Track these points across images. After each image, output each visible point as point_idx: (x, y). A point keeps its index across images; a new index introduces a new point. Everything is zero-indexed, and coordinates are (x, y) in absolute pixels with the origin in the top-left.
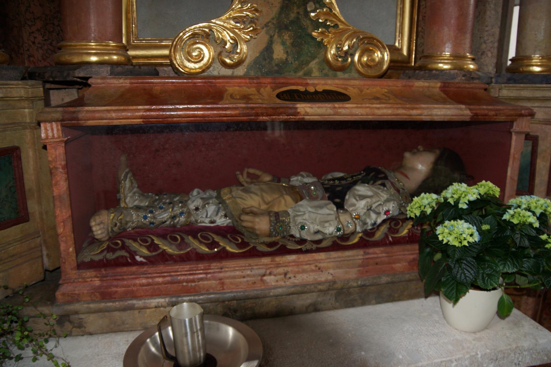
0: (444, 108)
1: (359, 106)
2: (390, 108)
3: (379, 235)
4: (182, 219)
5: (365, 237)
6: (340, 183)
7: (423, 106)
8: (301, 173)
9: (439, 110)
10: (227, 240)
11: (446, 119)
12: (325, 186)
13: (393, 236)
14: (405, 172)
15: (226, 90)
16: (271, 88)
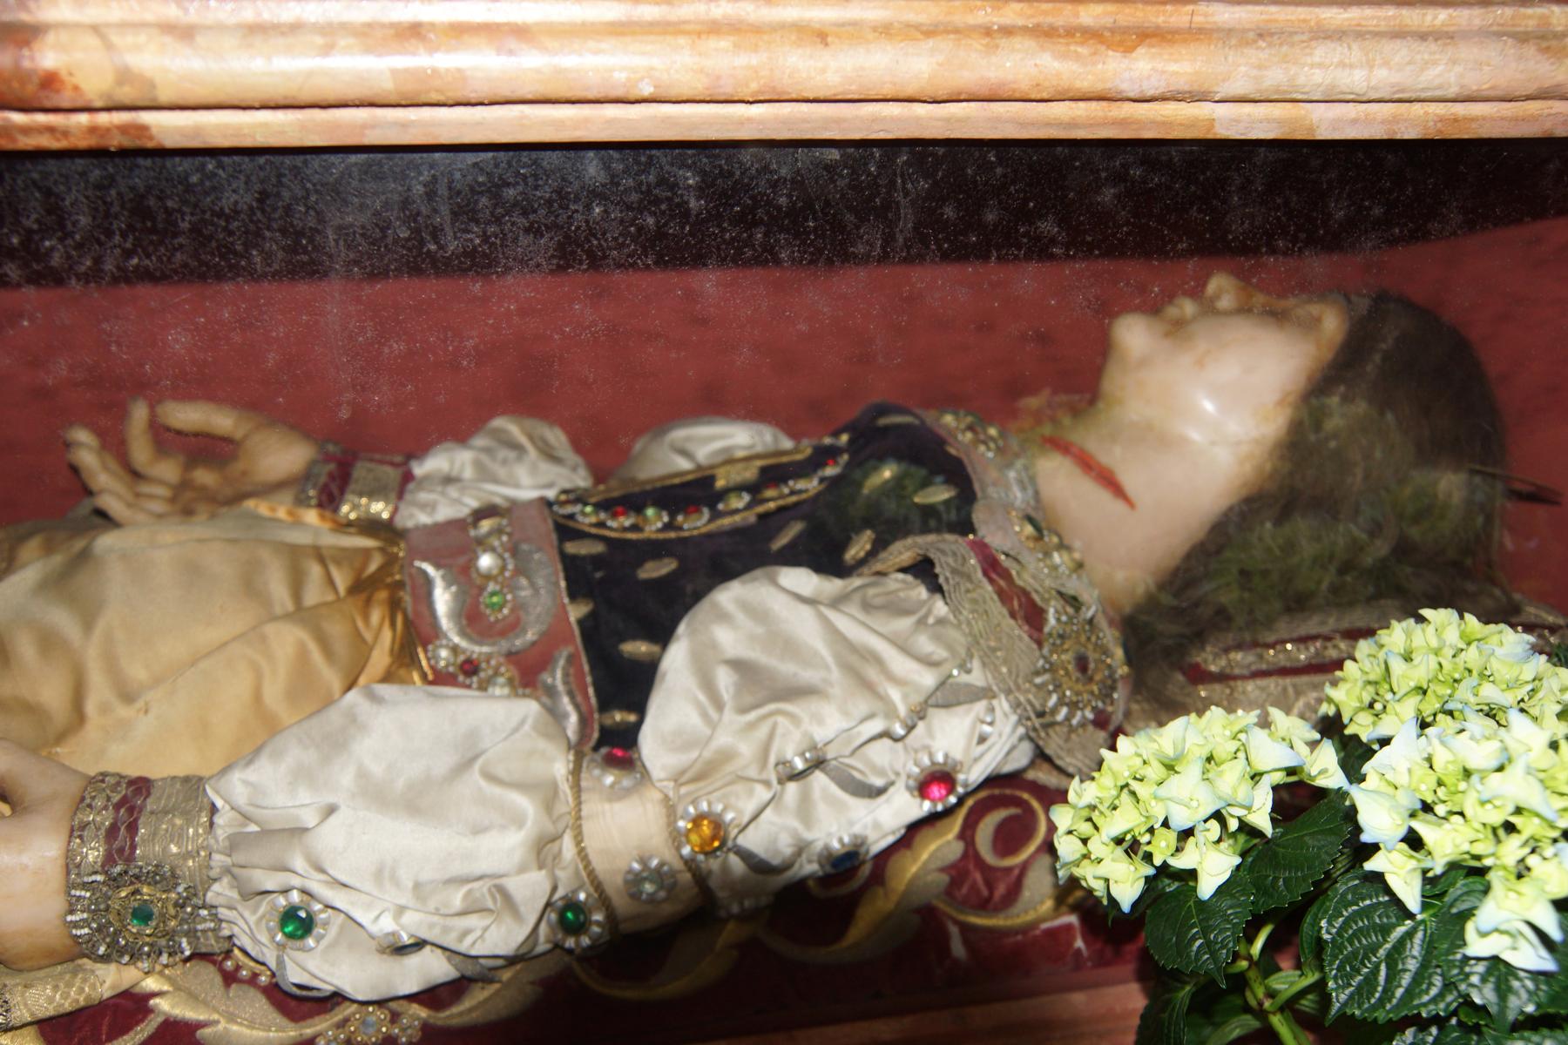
0: (1399, 34)
2: (930, 32)
6: (668, 527)
8: (499, 422)
9: (1355, 52)
11: (1412, 123)
12: (572, 548)
14: (1112, 456)
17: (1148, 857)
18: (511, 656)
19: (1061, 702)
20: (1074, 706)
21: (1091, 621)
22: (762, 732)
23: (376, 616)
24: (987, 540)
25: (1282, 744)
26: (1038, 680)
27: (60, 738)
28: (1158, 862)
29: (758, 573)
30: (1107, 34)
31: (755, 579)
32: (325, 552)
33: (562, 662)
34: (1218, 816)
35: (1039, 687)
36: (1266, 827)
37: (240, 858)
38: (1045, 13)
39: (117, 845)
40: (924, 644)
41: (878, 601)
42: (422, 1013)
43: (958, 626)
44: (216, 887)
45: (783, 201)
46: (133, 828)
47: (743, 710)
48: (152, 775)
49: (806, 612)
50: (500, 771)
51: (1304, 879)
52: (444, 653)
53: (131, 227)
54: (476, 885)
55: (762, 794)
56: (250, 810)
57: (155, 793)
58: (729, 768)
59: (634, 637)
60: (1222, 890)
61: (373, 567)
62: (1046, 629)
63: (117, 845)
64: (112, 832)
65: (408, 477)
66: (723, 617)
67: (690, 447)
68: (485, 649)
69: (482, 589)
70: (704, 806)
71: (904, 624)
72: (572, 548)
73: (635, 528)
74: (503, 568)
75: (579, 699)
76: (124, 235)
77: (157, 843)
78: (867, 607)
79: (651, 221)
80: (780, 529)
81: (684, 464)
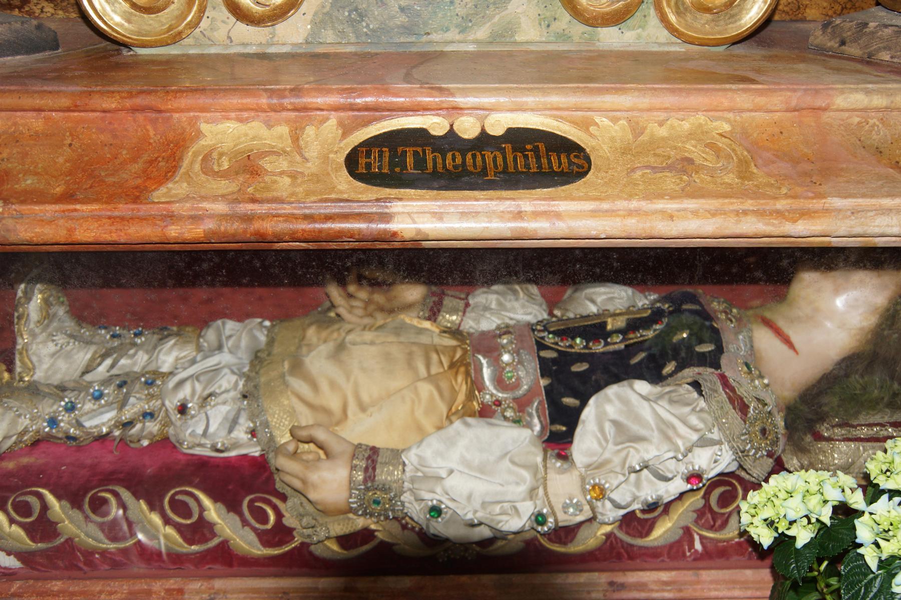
1: (605, 206)
3: (663, 531)
4: (153, 427)
5: (622, 535)
6: (586, 347)
7: (837, 202)
10: (237, 518)
12: (543, 354)
13: (705, 533)
15: (199, 134)
16: (341, 124)
17: (776, 529)
18: (515, 399)
19: (752, 447)
20: (758, 449)
21: (770, 412)
22: (623, 454)
23: (460, 378)
24: (726, 374)
25: (839, 488)
26: (743, 438)
27: (338, 423)
28: (780, 531)
29: (625, 383)
30: (787, 214)
31: (623, 386)
32: (438, 348)
33: (536, 404)
34: (807, 516)
35: (743, 441)
36: (828, 522)
37: (416, 486)
38: (762, 204)
39: (368, 474)
40: (694, 420)
41: (675, 399)
42: (478, 549)
43: (709, 413)
44: (405, 495)
45: (650, 264)
46: (374, 469)
47: (616, 444)
48: (377, 446)
49: (645, 404)
50: (516, 460)
51: (840, 546)
52: (488, 397)
53: (407, 269)
54: (505, 504)
55: (622, 478)
56: (419, 467)
57: (381, 454)
58: (609, 466)
59: (568, 396)
60: (805, 546)
61: (458, 355)
62: (749, 415)
63: (368, 474)
64: (366, 469)
65: (467, 305)
66: (609, 400)
67: (594, 297)
68: (505, 396)
69: (504, 369)
70: (597, 481)
71: (687, 409)
72: (543, 354)
73: (571, 346)
74: (514, 361)
75: (542, 419)
76: (404, 271)
77: (383, 475)
78: (671, 402)
79: (598, 270)
80: (635, 354)
81: (593, 309)
